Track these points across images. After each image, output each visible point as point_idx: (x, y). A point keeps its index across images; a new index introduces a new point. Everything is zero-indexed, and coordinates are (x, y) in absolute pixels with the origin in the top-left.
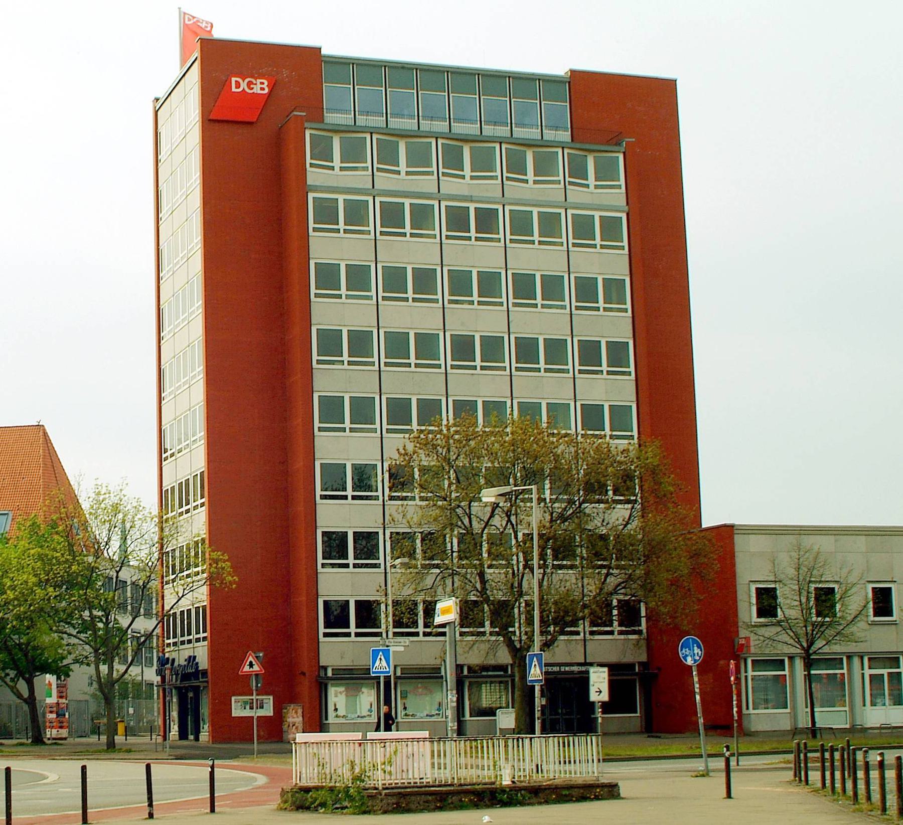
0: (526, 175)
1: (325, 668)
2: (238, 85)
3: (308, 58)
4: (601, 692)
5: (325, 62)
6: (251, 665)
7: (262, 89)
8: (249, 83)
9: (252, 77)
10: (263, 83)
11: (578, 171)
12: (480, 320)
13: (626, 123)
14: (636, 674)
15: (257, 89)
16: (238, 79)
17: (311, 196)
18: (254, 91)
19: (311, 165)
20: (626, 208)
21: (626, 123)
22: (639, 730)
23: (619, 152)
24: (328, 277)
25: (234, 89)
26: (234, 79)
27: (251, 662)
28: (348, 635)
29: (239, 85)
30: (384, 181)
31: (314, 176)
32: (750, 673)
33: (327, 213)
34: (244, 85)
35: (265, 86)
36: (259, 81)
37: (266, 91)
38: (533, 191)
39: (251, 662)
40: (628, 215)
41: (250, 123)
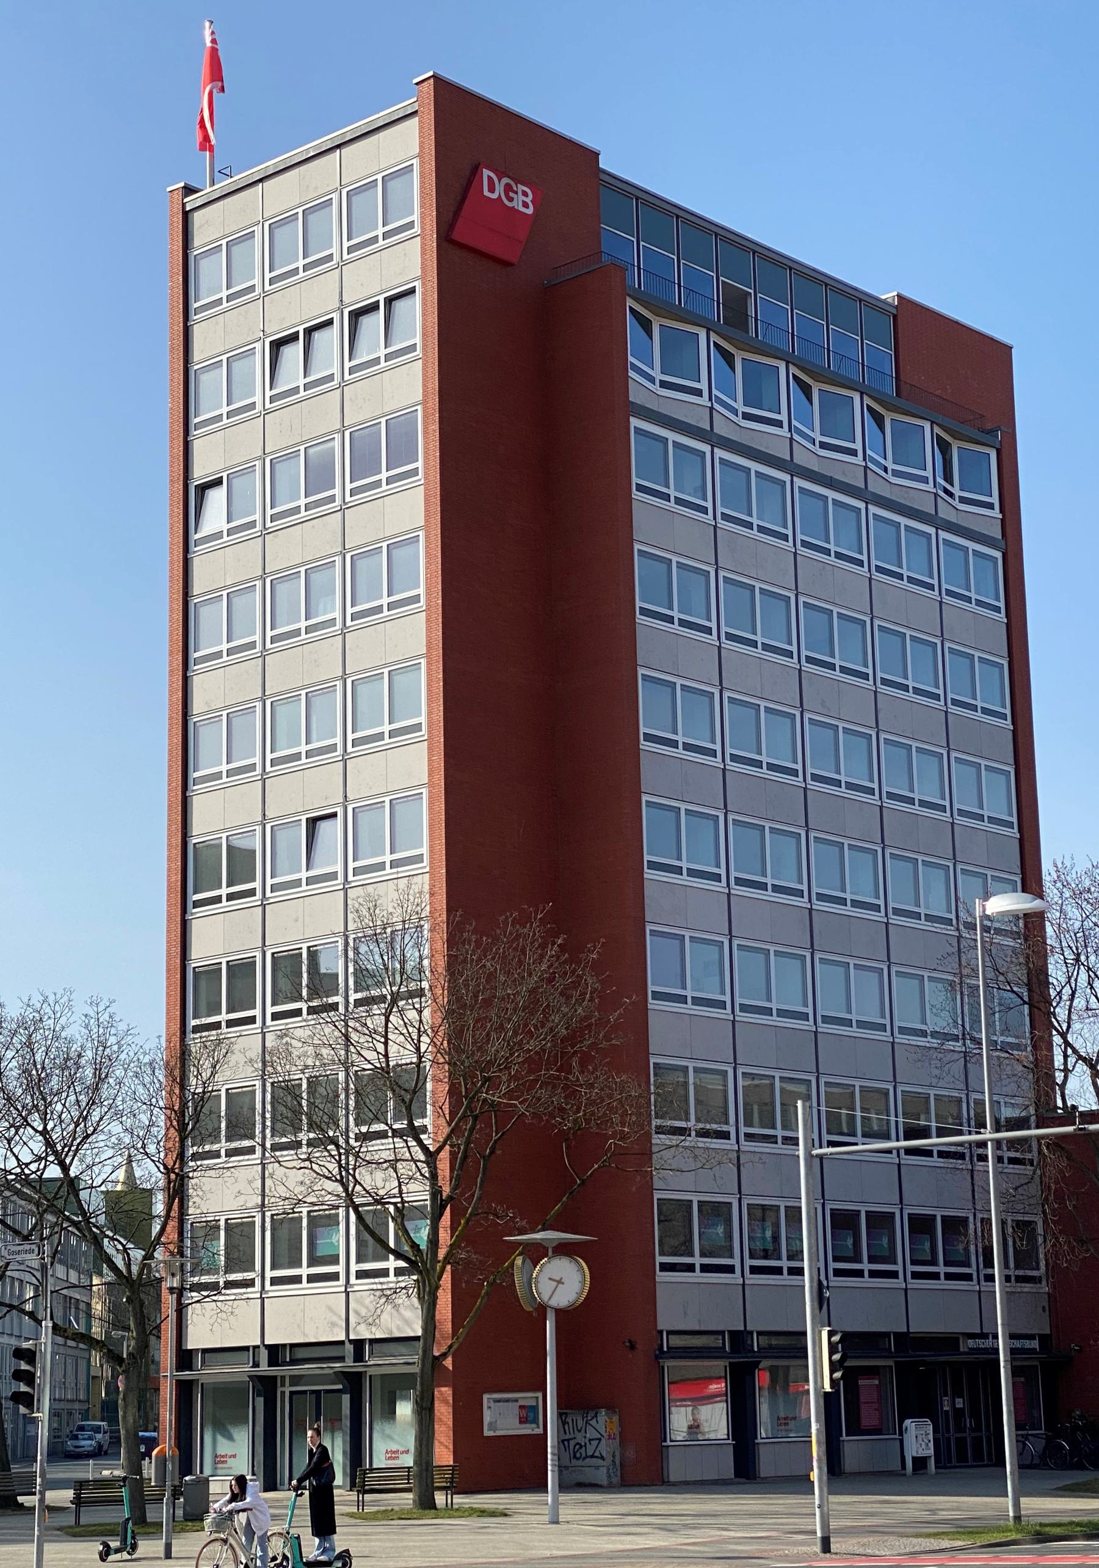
2: (492, 189)
7: (526, 205)
8: (508, 188)
13: (950, 383)
15: (517, 203)
34: (499, 189)
35: (528, 200)
36: (521, 188)
41: (507, 264)
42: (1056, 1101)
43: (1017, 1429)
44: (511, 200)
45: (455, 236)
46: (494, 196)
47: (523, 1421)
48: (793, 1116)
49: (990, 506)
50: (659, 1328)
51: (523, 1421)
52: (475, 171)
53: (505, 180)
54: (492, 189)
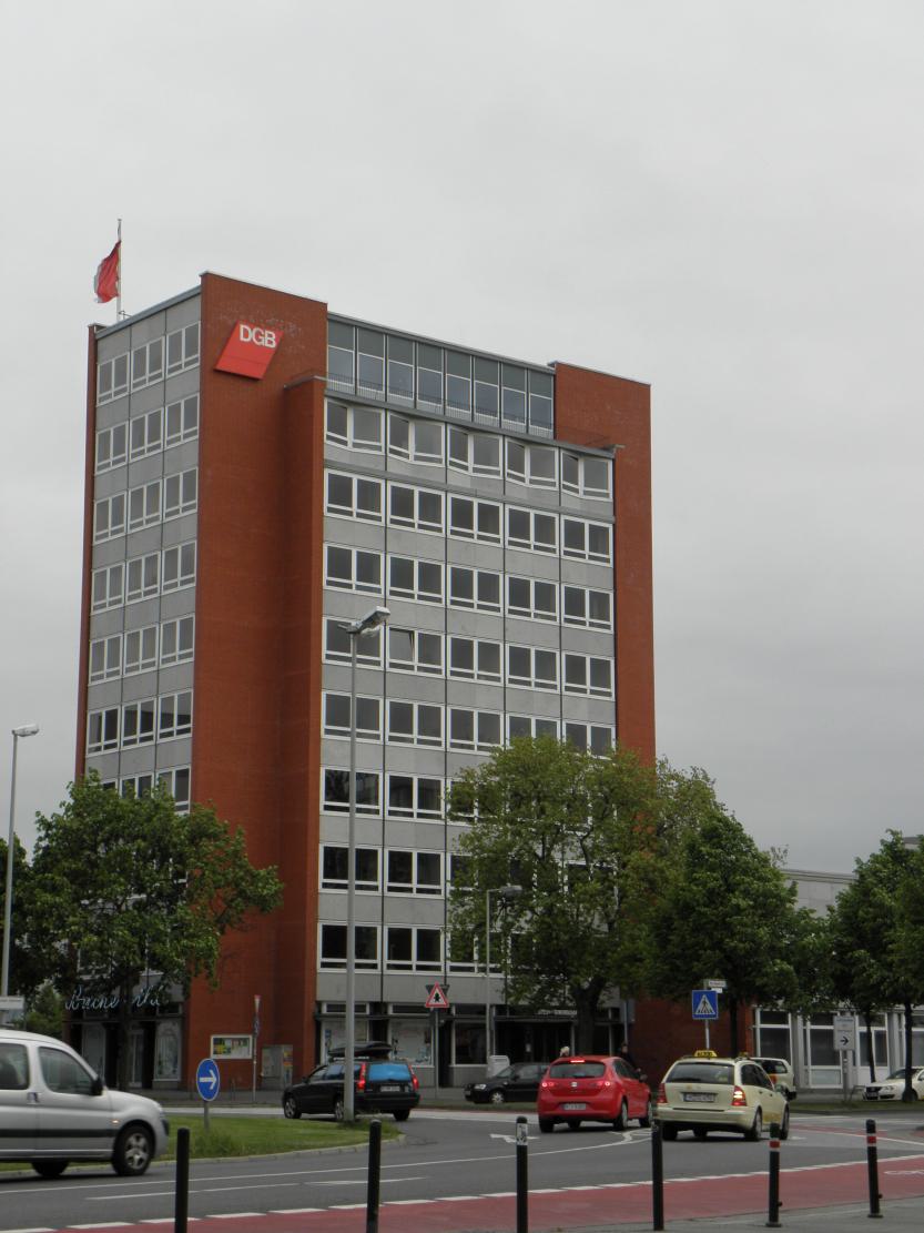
0: (577, 484)
1: (319, 1004)
2: (246, 335)
3: (313, 312)
4: (847, 1041)
5: (330, 320)
6: (437, 998)
7: (270, 342)
8: (258, 334)
9: (261, 327)
10: (270, 336)
11: (570, 475)
12: (482, 623)
13: (599, 419)
14: (610, 1021)
15: (265, 342)
16: (247, 327)
17: (327, 472)
18: (262, 343)
19: (329, 438)
20: (613, 519)
21: (599, 419)
22: (432, 1084)
23: (609, 458)
24: (340, 563)
25: (242, 338)
26: (242, 327)
27: (437, 995)
28: (409, 967)
29: (247, 334)
30: (396, 465)
31: (331, 449)
32: (759, 1026)
33: (341, 491)
34: (252, 335)
35: (273, 339)
36: (267, 332)
37: (274, 345)
38: (525, 488)
39: (437, 995)
40: (614, 525)
41: (255, 380)
42: (261, 1002)
43: (344, 1017)
44: (260, 340)
45: (225, 364)
46: (248, 340)
47: (329, 852)
48: (751, 1015)
49: (607, 561)
50: (319, 998)
51: (329, 852)
52: (236, 325)
53: (256, 330)
54: (246, 335)
